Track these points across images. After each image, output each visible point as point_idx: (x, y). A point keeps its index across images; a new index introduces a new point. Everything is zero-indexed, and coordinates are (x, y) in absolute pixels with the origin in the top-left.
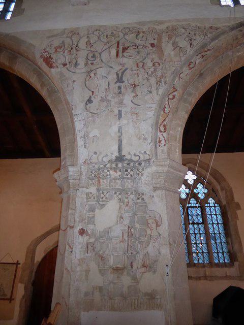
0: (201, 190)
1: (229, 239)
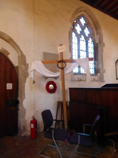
0: (87, 32)
1: (96, 62)
